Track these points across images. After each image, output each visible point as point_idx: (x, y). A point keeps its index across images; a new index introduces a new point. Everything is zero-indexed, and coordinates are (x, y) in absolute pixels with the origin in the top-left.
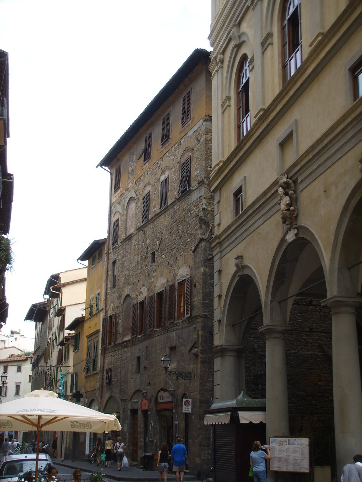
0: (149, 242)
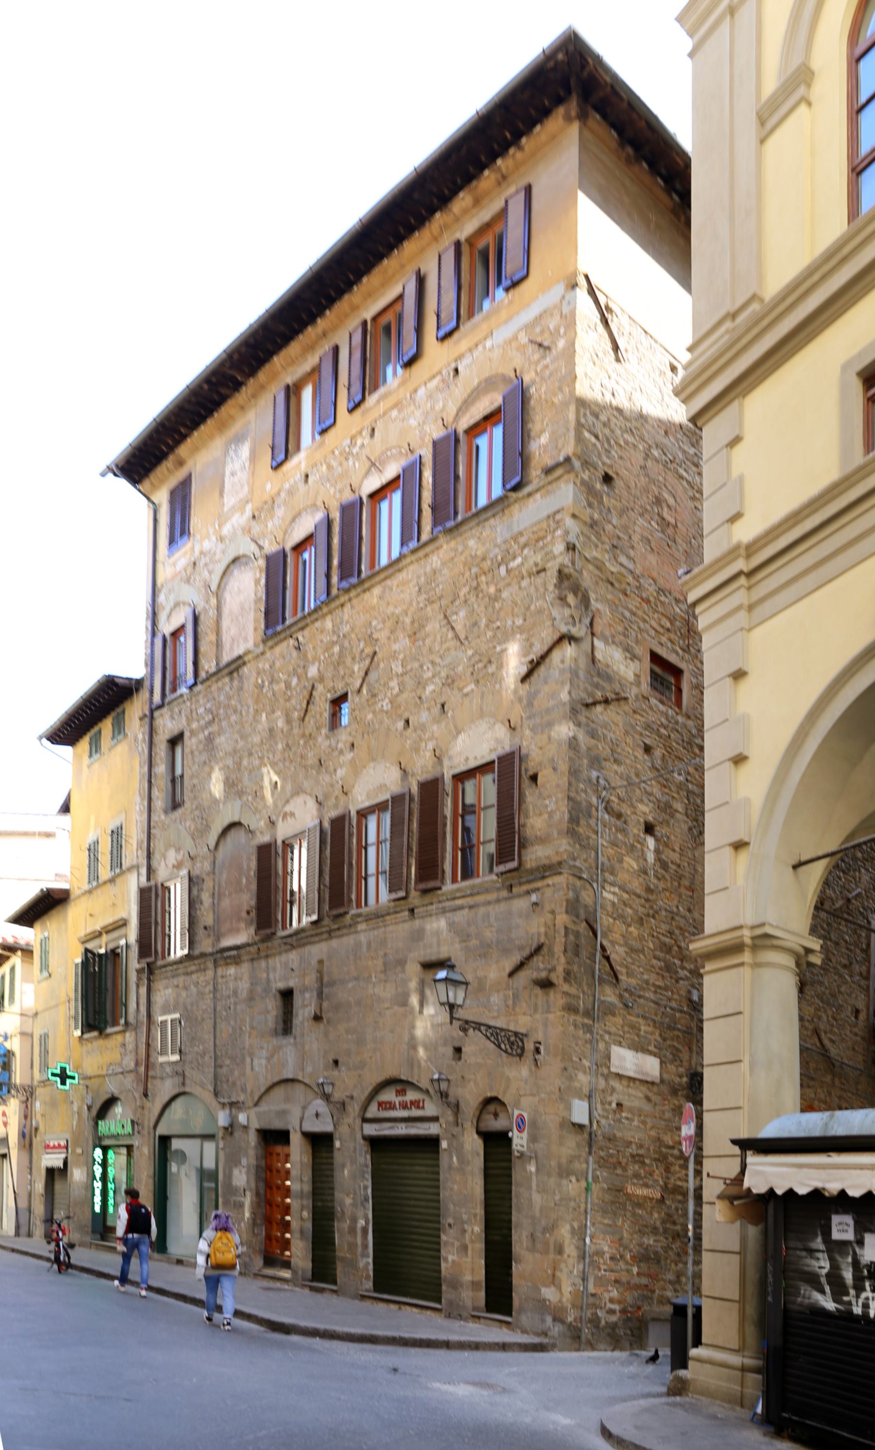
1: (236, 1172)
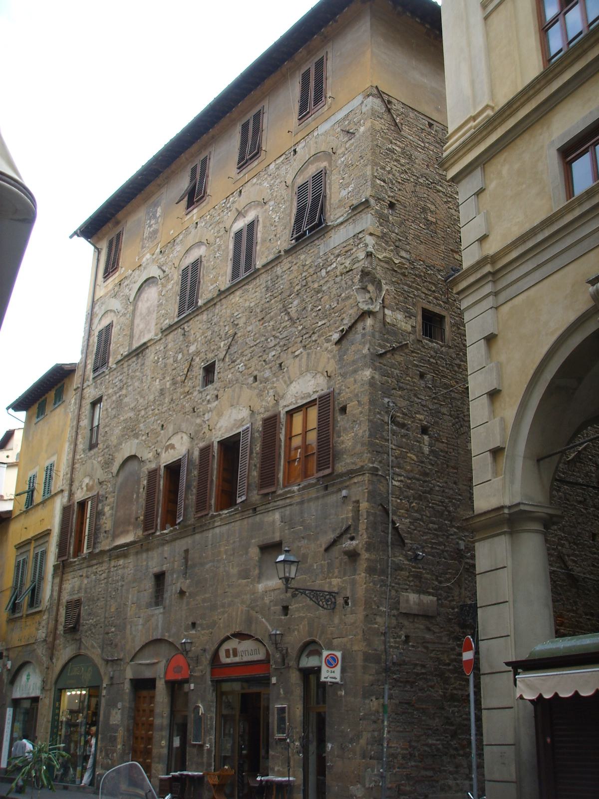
0: (197, 349)
1: (113, 712)
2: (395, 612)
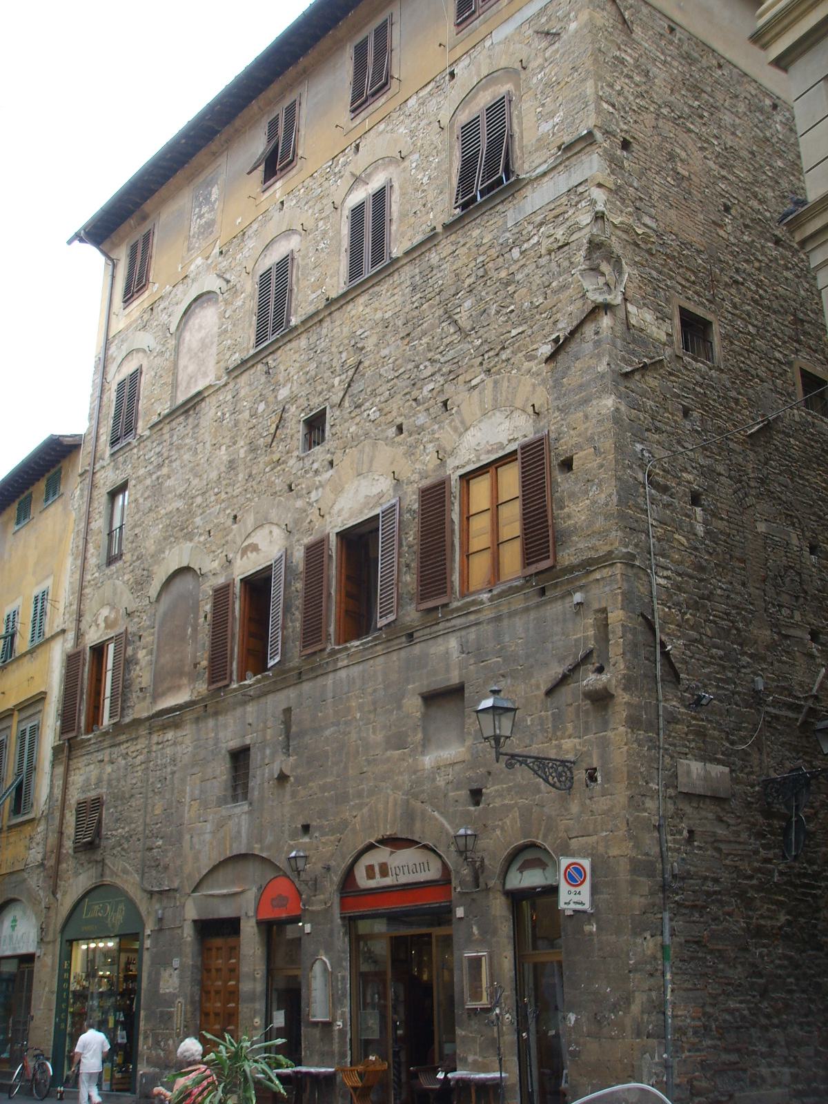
1: (165, 974)
2: (671, 792)
